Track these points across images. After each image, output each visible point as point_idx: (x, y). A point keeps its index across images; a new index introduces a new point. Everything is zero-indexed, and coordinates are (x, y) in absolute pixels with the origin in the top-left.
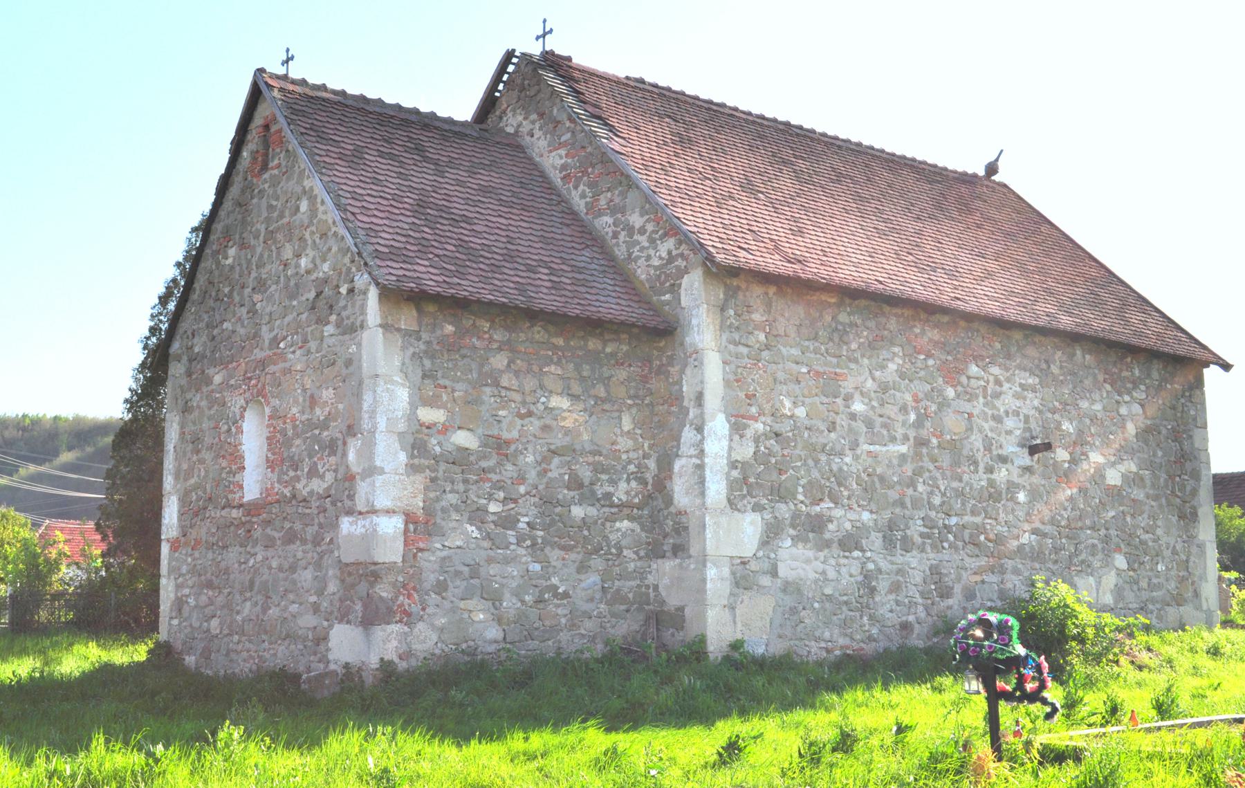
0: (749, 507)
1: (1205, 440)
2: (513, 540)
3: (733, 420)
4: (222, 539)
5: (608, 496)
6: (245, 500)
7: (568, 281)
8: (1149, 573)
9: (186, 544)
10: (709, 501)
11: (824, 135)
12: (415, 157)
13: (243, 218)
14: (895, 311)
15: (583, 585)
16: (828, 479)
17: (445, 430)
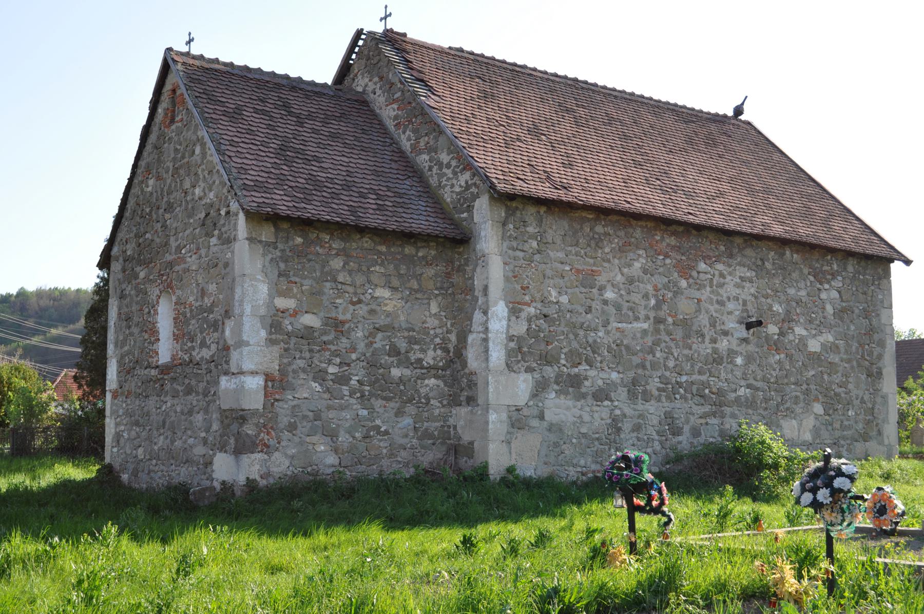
0: (523, 369)
1: (891, 317)
2: (347, 393)
3: (511, 305)
4: (145, 391)
5: (420, 361)
6: (160, 363)
7: (390, 204)
8: (841, 417)
9: (122, 394)
10: (491, 365)
11: (605, 87)
12: (282, 112)
13: (159, 157)
14: (640, 223)
15: (400, 425)
16: (585, 348)
17: (295, 314)
